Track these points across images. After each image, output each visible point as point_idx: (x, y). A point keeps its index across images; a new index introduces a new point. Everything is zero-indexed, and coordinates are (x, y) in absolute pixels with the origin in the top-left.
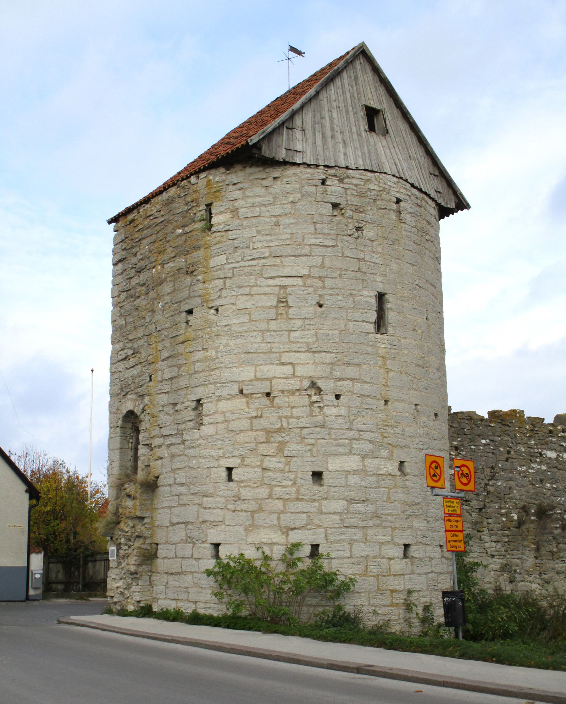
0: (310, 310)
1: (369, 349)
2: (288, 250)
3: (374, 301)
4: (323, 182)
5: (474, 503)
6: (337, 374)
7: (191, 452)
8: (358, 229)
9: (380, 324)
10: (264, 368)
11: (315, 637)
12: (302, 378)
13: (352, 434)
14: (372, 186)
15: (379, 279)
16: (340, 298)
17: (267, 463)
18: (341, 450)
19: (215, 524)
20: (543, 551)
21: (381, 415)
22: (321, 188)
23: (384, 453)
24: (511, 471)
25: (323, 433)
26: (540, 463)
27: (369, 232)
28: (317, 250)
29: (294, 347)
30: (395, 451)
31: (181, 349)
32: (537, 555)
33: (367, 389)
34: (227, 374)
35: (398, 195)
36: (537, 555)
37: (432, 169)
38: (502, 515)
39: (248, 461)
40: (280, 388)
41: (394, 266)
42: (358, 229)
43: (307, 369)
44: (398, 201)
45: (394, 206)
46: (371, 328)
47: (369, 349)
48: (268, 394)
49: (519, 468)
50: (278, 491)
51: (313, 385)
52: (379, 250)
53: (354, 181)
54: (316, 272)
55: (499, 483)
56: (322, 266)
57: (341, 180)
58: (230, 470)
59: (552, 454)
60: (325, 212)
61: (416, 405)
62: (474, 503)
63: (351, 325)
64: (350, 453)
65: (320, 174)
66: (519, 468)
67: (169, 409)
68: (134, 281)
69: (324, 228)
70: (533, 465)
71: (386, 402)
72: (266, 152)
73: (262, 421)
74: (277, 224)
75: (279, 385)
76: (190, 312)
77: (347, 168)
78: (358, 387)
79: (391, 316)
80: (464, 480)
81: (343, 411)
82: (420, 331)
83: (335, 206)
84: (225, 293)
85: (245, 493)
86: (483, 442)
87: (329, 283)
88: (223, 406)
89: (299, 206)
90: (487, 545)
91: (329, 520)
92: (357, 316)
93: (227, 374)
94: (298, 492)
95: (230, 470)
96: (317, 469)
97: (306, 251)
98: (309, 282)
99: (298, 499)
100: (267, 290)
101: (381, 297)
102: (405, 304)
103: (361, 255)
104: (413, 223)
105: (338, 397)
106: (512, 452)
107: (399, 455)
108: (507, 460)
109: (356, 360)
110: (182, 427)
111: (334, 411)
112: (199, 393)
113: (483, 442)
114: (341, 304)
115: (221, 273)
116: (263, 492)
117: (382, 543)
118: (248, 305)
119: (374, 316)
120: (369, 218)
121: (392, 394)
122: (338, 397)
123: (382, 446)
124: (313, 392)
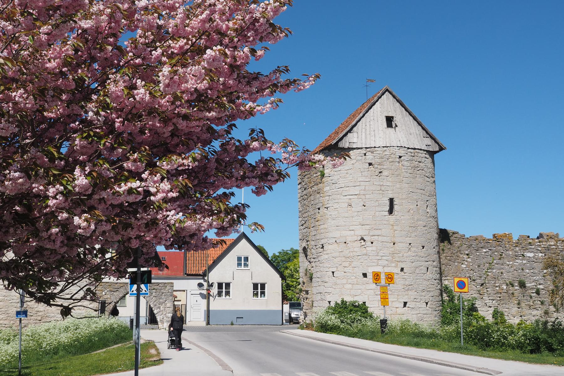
0: (361, 208)
1: (385, 222)
2: (352, 184)
3: (388, 203)
4: (365, 155)
5: (478, 281)
6: (371, 234)
7: (321, 265)
8: (380, 172)
9: (391, 211)
10: (343, 232)
11: (412, 343)
12: (357, 236)
13: (378, 258)
14: (386, 153)
15: (391, 192)
16: (372, 202)
17: (346, 270)
18: (374, 264)
19: (329, 293)
20: (523, 305)
21: (393, 249)
22: (364, 157)
23: (393, 265)
24: (502, 265)
25: (366, 257)
26: (522, 260)
27: (385, 173)
28: (362, 183)
29: (354, 223)
30: (399, 263)
31: (317, 223)
32: (518, 306)
33: (385, 239)
34: (330, 235)
35: (400, 155)
36: (518, 306)
37: (425, 135)
38: (496, 287)
39: (339, 269)
40: (349, 240)
41: (398, 186)
42: (380, 172)
43: (361, 232)
44: (400, 157)
45: (398, 160)
46: (387, 213)
47: (385, 222)
48: (345, 243)
49: (508, 263)
50: (350, 281)
51: (362, 239)
52: (390, 180)
53: (378, 152)
54: (362, 192)
55: (494, 271)
56: (365, 190)
57: (372, 152)
58: (333, 272)
59: (531, 255)
60: (365, 167)
61: (410, 244)
62: (478, 281)
63: (377, 213)
64: (378, 265)
65: (363, 151)
66: (508, 263)
67: (314, 247)
68: (304, 193)
69: (365, 174)
70: (517, 261)
71: (394, 244)
72: (341, 145)
73: (343, 253)
74: (347, 173)
75: (348, 240)
76: (319, 209)
77: (375, 147)
78: (380, 238)
79: (396, 207)
80: (390, 280)
81: (374, 248)
82: (412, 212)
83: (370, 164)
84: (329, 202)
85: (339, 281)
86: (485, 250)
87: (367, 196)
88: (330, 247)
89: (355, 165)
90: (486, 301)
91: (369, 292)
92: (380, 209)
93: (330, 235)
94: (357, 281)
95: (333, 272)
96: (364, 272)
97: (358, 184)
98: (360, 197)
99: (357, 284)
100: (344, 201)
101: (391, 201)
102: (403, 201)
103: (382, 184)
104: (409, 165)
105: (372, 243)
106: (504, 255)
107: (401, 265)
108: (500, 259)
109: (379, 228)
110: (318, 255)
111: (371, 249)
112: (323, 242)
113: (485, 250)
114: (373, 205)
115: (328, 194)
116: (344, 281)
117: (393, 301)
118: (337, 207)
119: (388, 208)
120: (385, 167)
121: (396, 240)
122: (372, 243)
123: (392, 262)
124: (362, 241)
